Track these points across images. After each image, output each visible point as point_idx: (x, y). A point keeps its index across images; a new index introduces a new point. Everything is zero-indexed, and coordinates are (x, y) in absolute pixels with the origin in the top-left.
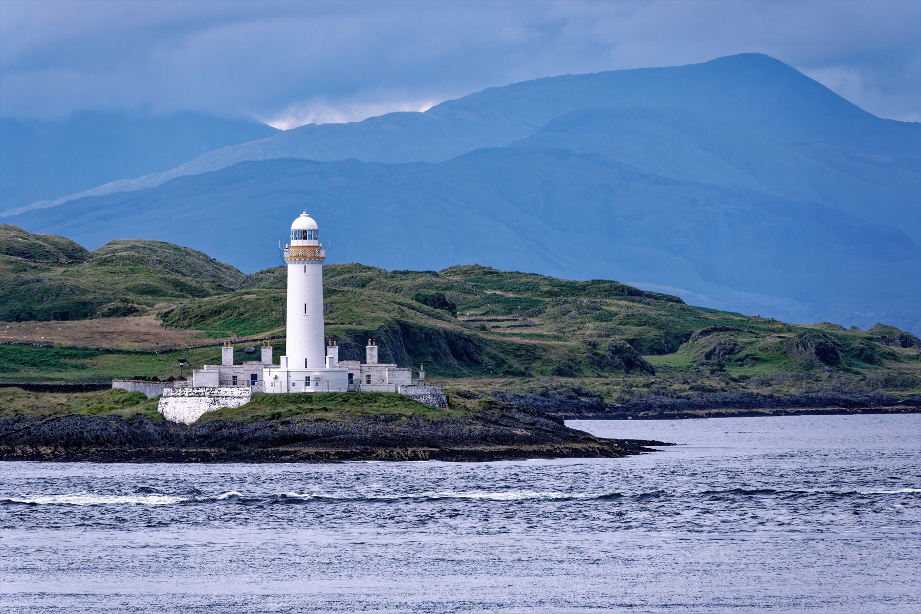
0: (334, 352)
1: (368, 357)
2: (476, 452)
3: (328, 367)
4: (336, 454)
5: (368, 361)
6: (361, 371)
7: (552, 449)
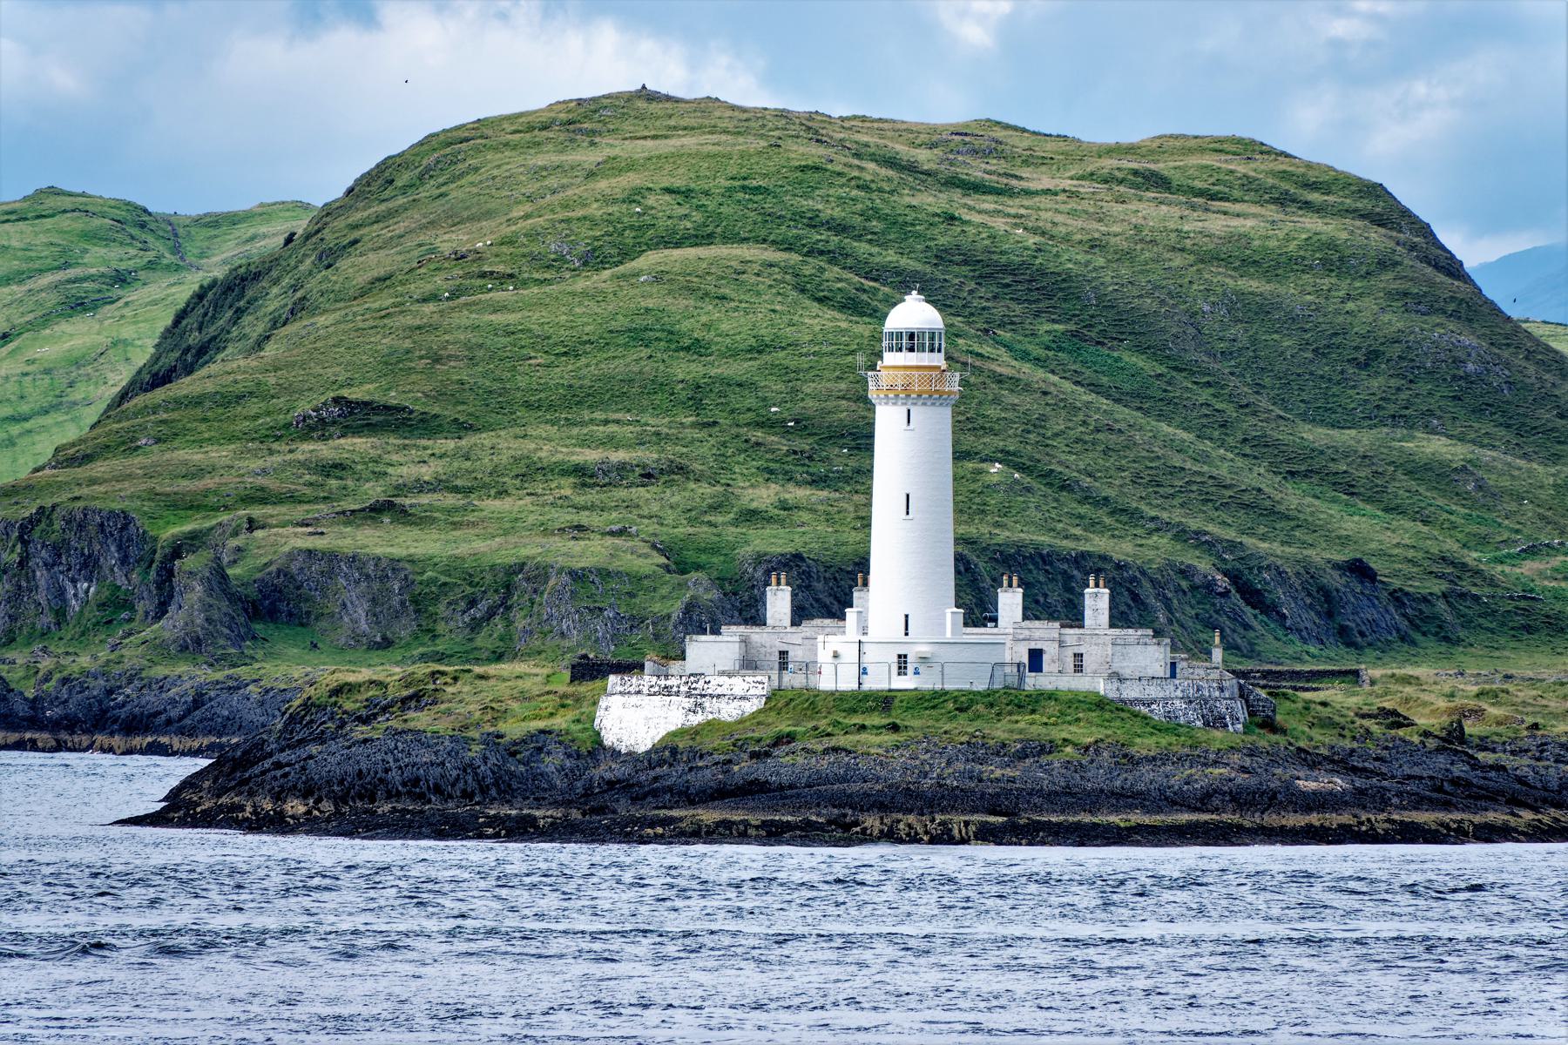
0: (1010, 601)
1: (1088, 613)
2: (1078, 826)
3: (949, 634)
4: (764, 824)
5: (1087, 622)
6: (1062, 644)
7: (1353, 821)
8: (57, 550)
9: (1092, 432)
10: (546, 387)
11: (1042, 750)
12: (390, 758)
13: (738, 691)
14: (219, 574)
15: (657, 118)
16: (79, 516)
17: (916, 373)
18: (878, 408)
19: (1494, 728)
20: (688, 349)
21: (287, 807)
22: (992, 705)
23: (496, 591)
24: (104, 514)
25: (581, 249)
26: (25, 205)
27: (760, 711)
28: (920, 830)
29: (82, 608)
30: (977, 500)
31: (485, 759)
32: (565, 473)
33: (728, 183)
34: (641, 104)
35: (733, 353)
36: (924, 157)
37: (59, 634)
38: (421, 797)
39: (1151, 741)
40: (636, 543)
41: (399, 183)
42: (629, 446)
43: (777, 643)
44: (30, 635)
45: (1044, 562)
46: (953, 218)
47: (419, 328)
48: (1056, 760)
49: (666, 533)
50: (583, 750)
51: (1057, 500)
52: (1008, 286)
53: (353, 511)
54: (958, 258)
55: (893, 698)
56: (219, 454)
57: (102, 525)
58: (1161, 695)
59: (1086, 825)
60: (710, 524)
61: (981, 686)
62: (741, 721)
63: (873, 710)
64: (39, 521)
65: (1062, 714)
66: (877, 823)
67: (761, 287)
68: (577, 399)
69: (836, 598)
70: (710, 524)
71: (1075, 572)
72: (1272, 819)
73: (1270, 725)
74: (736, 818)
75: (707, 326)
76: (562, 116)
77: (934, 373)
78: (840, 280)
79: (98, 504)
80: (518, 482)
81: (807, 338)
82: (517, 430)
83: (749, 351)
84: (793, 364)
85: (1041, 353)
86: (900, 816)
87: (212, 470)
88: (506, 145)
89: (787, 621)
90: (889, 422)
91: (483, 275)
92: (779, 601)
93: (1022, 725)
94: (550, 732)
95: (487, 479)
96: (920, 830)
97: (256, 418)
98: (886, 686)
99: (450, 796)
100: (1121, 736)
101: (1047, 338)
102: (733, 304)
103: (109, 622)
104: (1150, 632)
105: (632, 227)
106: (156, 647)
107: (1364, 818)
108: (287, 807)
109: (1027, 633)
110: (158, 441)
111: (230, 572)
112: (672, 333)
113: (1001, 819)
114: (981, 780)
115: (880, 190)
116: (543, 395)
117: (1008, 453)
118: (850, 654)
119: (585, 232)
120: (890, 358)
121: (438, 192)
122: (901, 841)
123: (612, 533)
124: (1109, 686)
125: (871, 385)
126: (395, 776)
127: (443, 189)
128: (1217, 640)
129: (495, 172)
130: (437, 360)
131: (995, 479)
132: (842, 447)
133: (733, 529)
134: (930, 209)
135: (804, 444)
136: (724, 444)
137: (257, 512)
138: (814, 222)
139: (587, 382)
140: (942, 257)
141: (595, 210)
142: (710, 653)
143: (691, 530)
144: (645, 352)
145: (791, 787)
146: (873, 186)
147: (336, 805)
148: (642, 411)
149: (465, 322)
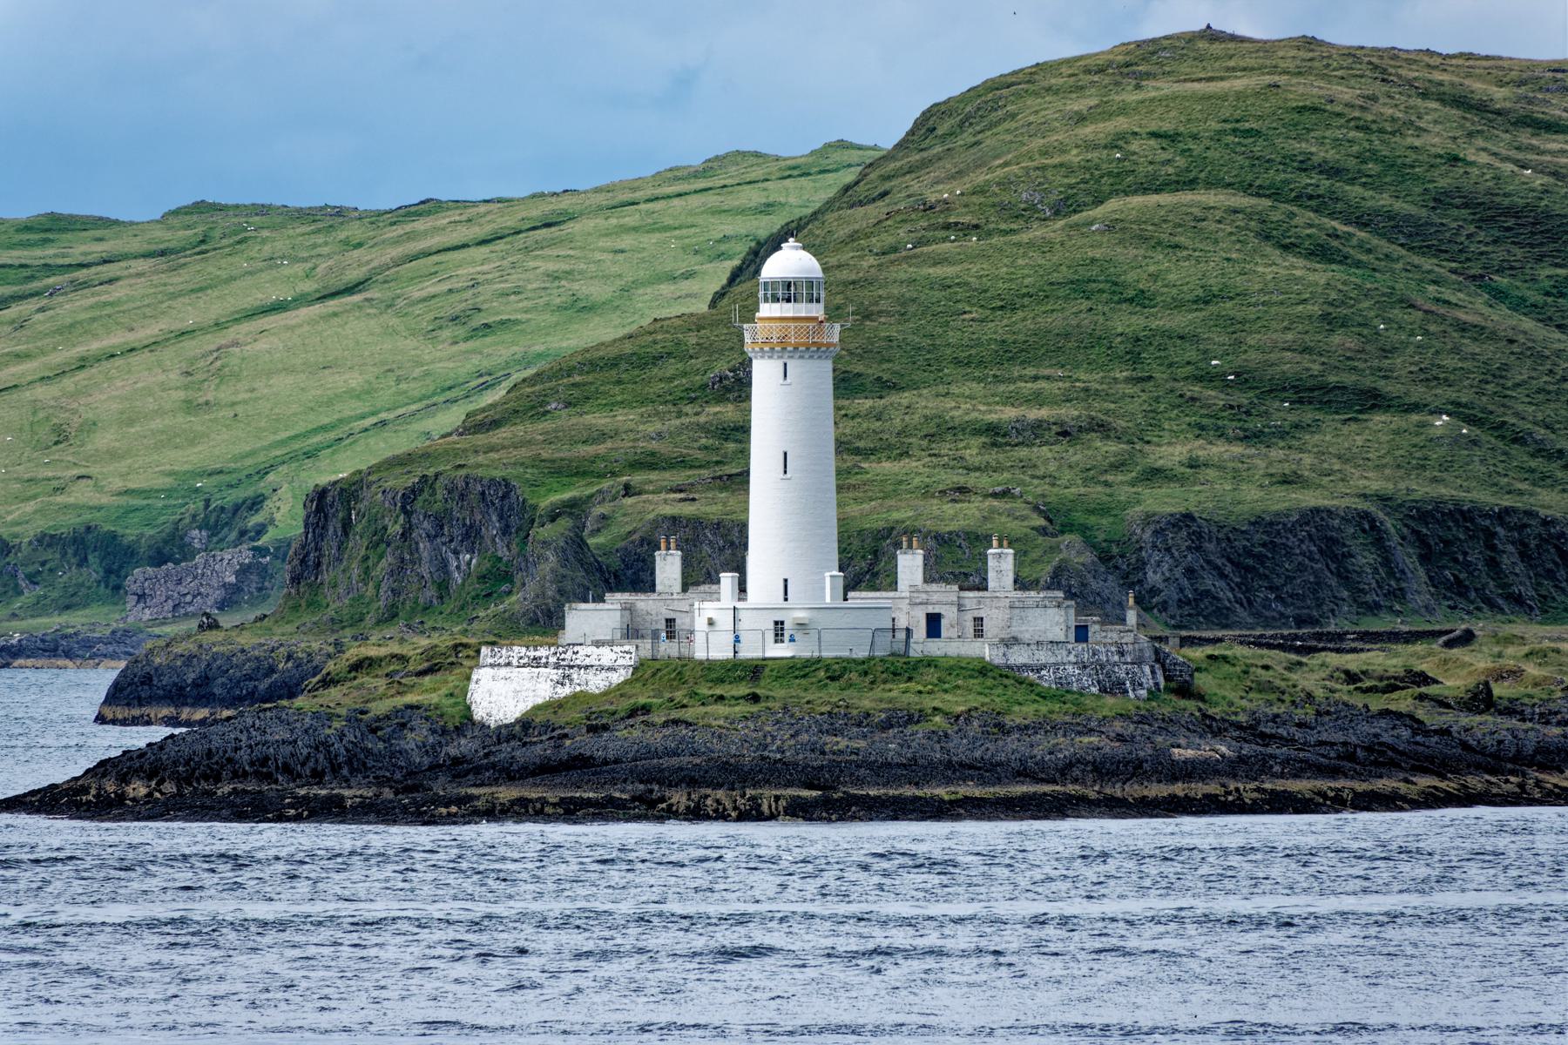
1: (991, 575)
3: (828, 600)
4: (563, 801)
5: (991, 585)
6: (961, 608)
7: (1219, 791)
8: (439, 522)
9: (1559, 381)
10: (979, 343)
11: (910, 720)
12: (244, 737)
13: (606, 662)
14: (578, 543)
15: (1217, 59)
16: (461, 484)
17: (792, 325)
19: (1530, 690)
20: (1131, 301)
21: (129, 790)
22: (866, 673)
23: (863, 557)
24: (485, 482)
25: (1054, 197)
26: (810, 160)
27: (626, 682)
28: (729, 805)
29: (464, 581)
30: (1418, 455)
31: (342, 736)
32: (977, 432)
33: (1219, 127)
34: (1201, 45)
35: (1178, 305)
36: (1501, 96)
37: (441, 608)
38: (269, 778)
39: (1029, 709)
40: (1019, 504)
41: (939, 132)
42: (1054, 403)
43: (664, 611)
45: (1465, 520)
46: (1456, 159)
47: (853, 282)
48: (921, 729)
49: (1054, 494)
50: (450, 727)
51: (1505, 453)
52: (1508, 229)
53: (730, 476)
54: (1458, 201)
55: (763, 667)
56: (624, 418)
57: (483, 493)
58: (1052, 660)
59: (906, 798)
60: (1106, 484)
61: (861, 653)
62: (605, 694)
63: (741, 679)
64: (422, 490)
66: (684, 799)
67: (1221, 234)
68: (1011, 353)
69: (1229, 560)
70: (1106, 484)
71: (1498, 529)
72: (1134, 790)
73: (1185, 690)
74: (534, 796)
75: (1154, 277)
76: (1120, 58)
77: (811, 325)
78: (1311, 226)
79: (480, 472)
80: (925, 443)
81: (1257, 287)
82: (942, 389)
83: (1195, 302)
84: (1239, 316)
85: (1539, 299)
86: (709, 791)
87: (615, 434)
88: (1049, 89)
89: (677, 587)
90: (764, 374)
91: (947, 227)
92: (668, 567)
93: (894, 694)
94: (418, 707)
95: (893, 440)
96: (729, 805)
97: (671, 379)
98: (759, 654)
99: (299, 776)
100: (999, 703)
101: (1547, 284)
102: (1185, 253)
103: (489, 595)
104: (1060, 594)
105: (1110, 174)
106: (504, 621)
107: (1232, 787)
108: (129, 790)
109: (924, 596)
110: (568, 404)
111: (591, 541)
112: (1116, 284)
113: (815, 793)
114: (823, 753)
115: (1381, 131)
116: (973, 352)
117: (1459, 405)
118: (725, 621)
119: (1060, 180)
120: (767, 310)
121: (973, 140)
122: (707, 818)
123: (995, 495)
124: (995, 652)
125: (748, 339)
126: (244, 756)
127: (980, 137)
128: (1131, 601)
129: (1032, 119)
130: (868, 316)
131: (1439, 433)
132: (1284, 401)
133: (1127, 488)
134: (1433, 150)
135: (1242, 398)
136: (1157, 400)
137: (637, 478)
138: (1305, 165)
139: (1021, 337)
140: (1440, 200)
141: (1074, 157)
142: (591, 621)
143: (1082, 490)
144: (1086, 304)
145: (616, 761)
146: (1374, 127)
147: (179, 788)
148: (1077, 367)
149: (903, 276)
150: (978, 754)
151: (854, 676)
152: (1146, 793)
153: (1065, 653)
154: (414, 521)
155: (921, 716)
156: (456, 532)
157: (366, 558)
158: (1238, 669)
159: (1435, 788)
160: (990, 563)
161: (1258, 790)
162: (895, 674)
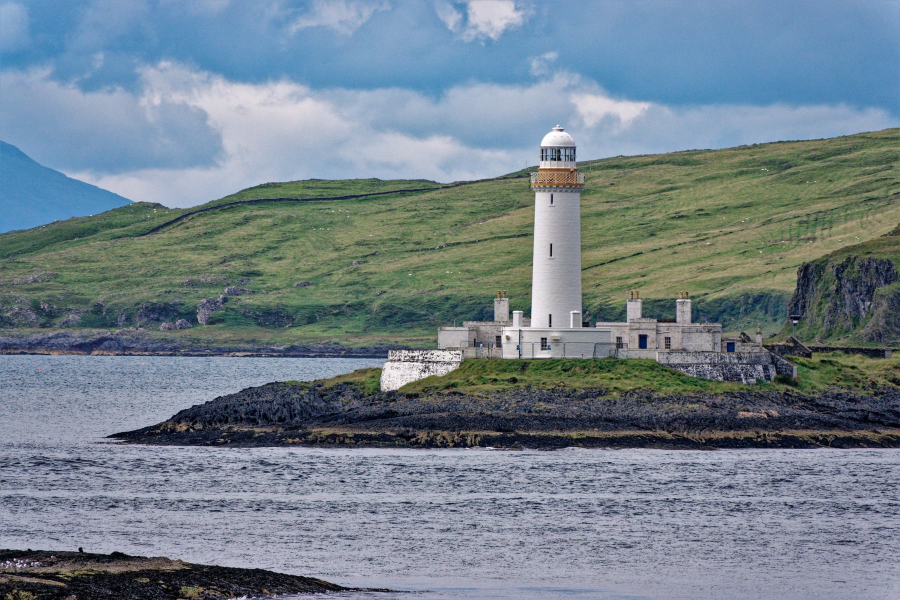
1: (678, 313)
5: (678, 319)
6: (658, 332)
11: (600, 394)
13: (447, 359)
16: (866, 263)
17: (556, 173)
18: (537, 194)
22: (585, 368)
43: (495, 331)
44: (840, 332)
58: (696, 361)
64: (847, 266)
65: (627, 372)
79: (876, 256)
86: (439, 432)
94: (351, 384)
109: (638, 325)
113: (498, 434)
114: (530, 412)
118: (515, 338)
124: (662, 357)
126: (242, 409)
150: (626, 413)
151: (577, 369)
152: (712, 436)
153: (703, 357)
154: (843, 283)
155: (607, 391)
156: (863, 289)
157: (821, 303)
158: (836, 368)
159: (891, 436)
160: (678, 307)
161: (776, 436)
162: (600, 368)
